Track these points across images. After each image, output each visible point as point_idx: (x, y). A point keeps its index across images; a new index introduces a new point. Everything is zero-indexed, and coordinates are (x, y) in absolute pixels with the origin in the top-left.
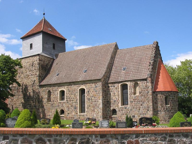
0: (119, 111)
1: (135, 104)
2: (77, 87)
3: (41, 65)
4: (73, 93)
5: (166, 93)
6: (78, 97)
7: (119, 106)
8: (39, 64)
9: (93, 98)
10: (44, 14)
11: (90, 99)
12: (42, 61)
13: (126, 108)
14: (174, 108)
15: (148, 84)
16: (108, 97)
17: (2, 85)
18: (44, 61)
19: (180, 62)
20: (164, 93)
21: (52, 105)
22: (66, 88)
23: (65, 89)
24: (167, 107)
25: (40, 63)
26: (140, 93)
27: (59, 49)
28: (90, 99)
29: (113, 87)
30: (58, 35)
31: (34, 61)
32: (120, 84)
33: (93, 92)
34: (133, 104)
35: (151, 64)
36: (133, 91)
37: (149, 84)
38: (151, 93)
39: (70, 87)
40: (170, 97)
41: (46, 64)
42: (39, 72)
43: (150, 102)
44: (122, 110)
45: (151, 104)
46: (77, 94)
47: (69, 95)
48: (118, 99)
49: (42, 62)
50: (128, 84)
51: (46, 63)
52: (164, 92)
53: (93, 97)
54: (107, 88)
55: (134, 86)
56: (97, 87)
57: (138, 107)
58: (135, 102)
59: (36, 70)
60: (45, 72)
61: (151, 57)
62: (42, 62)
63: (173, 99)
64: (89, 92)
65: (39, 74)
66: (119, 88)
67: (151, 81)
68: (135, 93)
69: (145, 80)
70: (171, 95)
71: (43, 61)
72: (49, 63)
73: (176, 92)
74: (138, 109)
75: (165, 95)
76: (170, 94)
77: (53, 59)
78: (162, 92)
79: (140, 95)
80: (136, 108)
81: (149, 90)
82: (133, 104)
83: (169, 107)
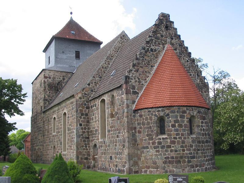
5: (159, 111)
10: (71, 13)
20: (154, 112)
24: (160, 139)
30: (86, 39)
40: (168, 118)
41: (57, 82)
51: (57, 80)
52: (154, 109)
63: (176, 121)
70: (170, 114)
72: (64, 79)
73: (188, 108)
76: (167, 112)
83: (166, 138)
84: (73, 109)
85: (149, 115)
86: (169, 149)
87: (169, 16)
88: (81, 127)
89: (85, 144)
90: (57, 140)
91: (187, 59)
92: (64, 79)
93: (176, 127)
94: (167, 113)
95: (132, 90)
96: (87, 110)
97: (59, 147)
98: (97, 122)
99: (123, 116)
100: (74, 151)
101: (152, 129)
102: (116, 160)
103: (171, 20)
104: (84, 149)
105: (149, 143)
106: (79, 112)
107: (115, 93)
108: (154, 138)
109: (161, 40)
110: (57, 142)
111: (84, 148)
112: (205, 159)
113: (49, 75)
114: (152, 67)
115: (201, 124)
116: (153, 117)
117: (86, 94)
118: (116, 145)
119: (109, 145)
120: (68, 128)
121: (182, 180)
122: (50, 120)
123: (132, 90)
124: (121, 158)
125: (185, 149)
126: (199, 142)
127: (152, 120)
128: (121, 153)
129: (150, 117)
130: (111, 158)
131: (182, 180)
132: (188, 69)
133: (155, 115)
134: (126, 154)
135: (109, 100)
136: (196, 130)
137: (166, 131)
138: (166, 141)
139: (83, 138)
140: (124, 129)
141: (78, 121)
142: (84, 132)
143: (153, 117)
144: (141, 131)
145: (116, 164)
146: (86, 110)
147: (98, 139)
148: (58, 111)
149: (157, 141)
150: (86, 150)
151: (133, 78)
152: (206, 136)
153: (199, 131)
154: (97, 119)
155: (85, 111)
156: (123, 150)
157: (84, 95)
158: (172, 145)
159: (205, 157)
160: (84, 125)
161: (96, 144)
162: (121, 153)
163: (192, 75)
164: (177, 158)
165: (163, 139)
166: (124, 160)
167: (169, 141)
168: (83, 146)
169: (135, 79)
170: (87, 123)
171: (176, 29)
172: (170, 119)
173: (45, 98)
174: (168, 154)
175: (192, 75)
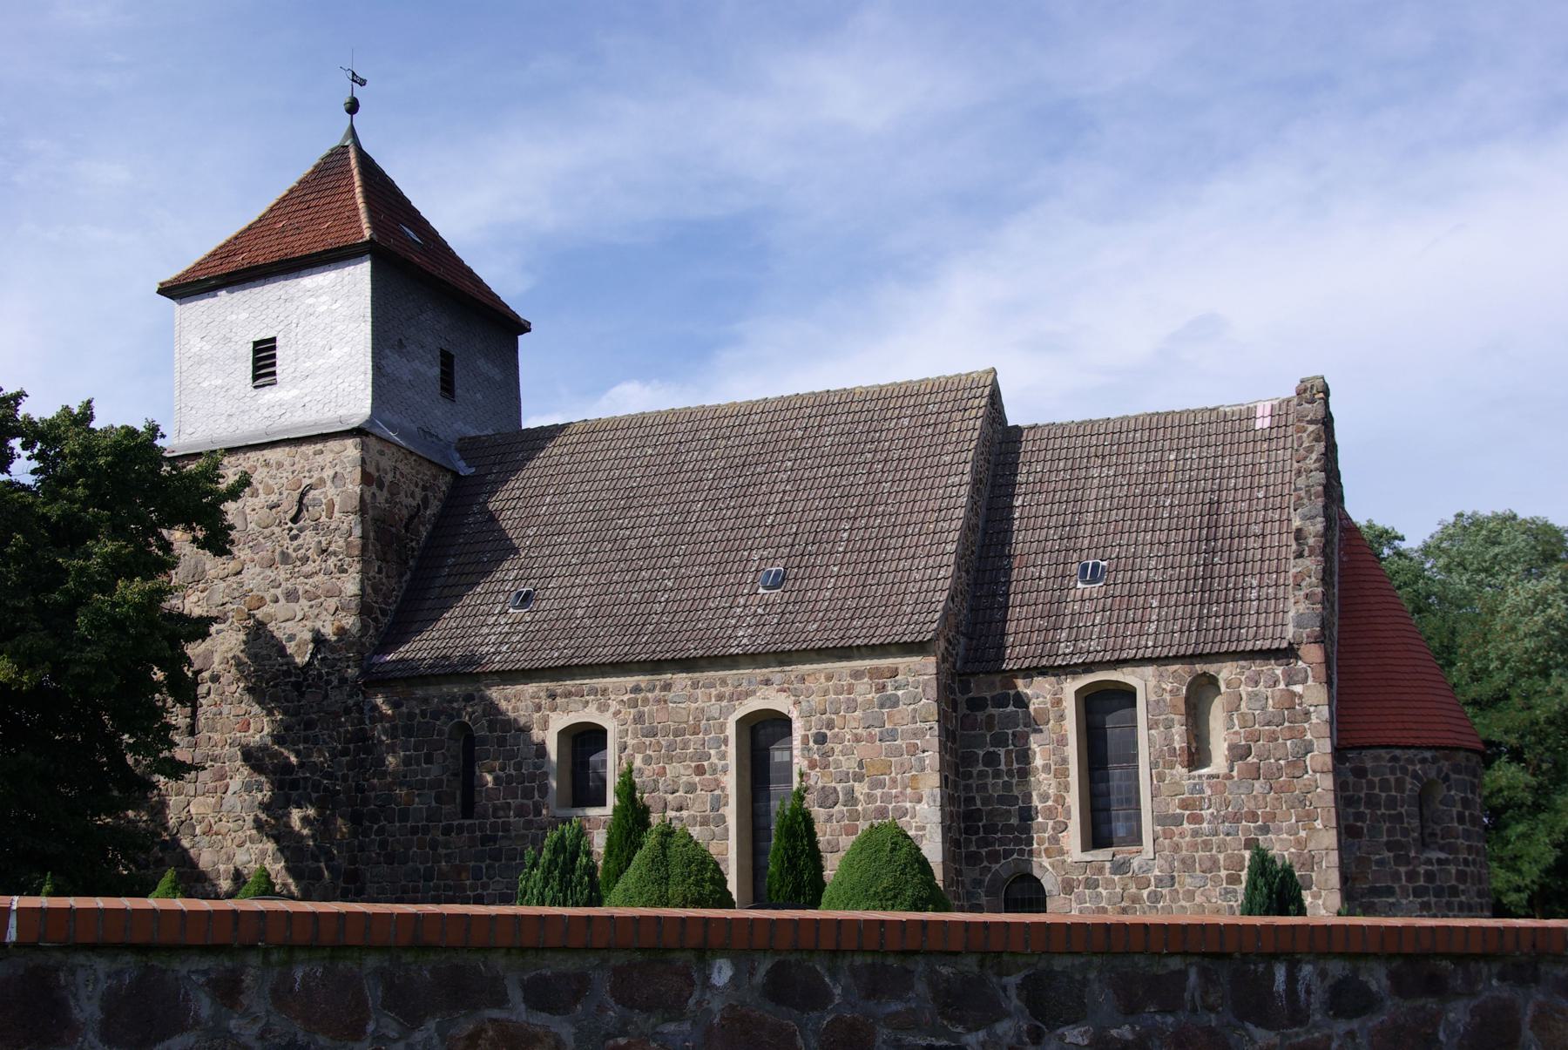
0: (1068, 887)
1: (1195, 833)
2: (720, 698)
3: (375, 520)
4: (685, 746)
6: (730, 781)
7: (1062, 852)
8: (363, 508)
9: (861, 789)
10: (353, 107)
11: (832, 797)
12: (381, 486)
13: (1120, 867)
14: (1472, 872)
15: (1298, 688)
16: (973, 782)
17: (1558, 628)
18: (394, 489)
19: (1400, 534)
21: (485, 840)
22: (614, 706)
23: (609, 714)
24: (1429, 862)
25: (368, 499)
26: (1238, 753)
27: (479, 396)
28: (832, 797)
29: (1011, 708)
31: (308, 481)
32: (1071, 686)
33: (857, 739)
34: (1182, 835)
35: (1311, 541)
36: (1176, 737)
37: (1314, 695)
38: (1329, 759)
39: (658, 701)
40: (1449, 788)
41: (405, 512)
42: (362, 571)
43: (1318, 824)
44: (1091, 884)
45: (1330, 839)
46: (723, 756)
47: (647, 760)
48: (1060, 800)
49: (382, 496)
50: (1137, 678)
52: (1411, 753)
53: (859, 778)
54: (965, 716)
55: (1187, 699)
56: (894, 701)
57: (1221, 857)
58: (1195, 819)
59: (335, 554)
60: (401, 575)
61: (1303, 493)
62: (378, 493)
64: (829, 745)
65: (362, 589)
66: (1062, 717)
67: (1322, 670)
68: (1197, 756)
69: (1288, 653)
70: (1454, 776)
71: (385, 489)
74: (1223, 873)
75: (1415, 776)
77: (448, 478)
78: (1398, 752)
79: (1235, 773)
80: (1208, 864)
81: (1309, 737)
82: (1182, 835)
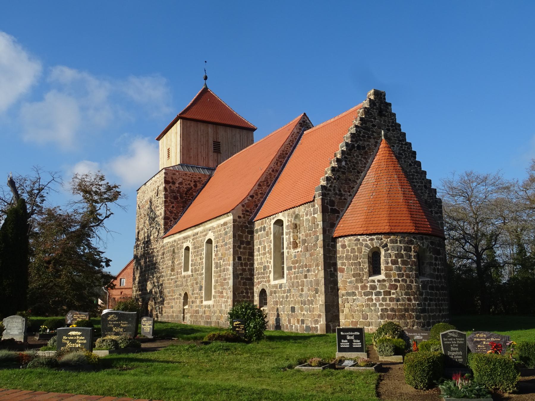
5: (372, 240)
10: (206, 78)
24: (373, 281)
76: (385, 240)
83: (384, 281)
84: (226, 233)
85: (356, 245)
86: (388, 297)
87: (385, 95)
88: (240, 262)
89: (246, 289)
90: (193, 283)
91: (410, 162)
92: (195, 186)
93: (398, 264)
94: (385, 242)
95: (330, 207)
96: (250, 236)
97: (197, 294)
98: (267, 254)
99: (315, 245)
100: (228, 299)
101: (361, 266)
102: (302, 313)
103: (387, 101)
104: (244, 297)
105: (357, 288)
106: (237, 238)
107: (302, 210)
108: (364, 280)
109: (373, 132)
110: (193, 286)
111: (244, 294)
112: (441, 314)
113: (172, 178)
114: (358, 172)
115: (434, 262)
116: (363, 248)
117: (247, 211)
118: (302, 290)
119: (289, 291)
120: (216, 264)
121: (422, 338)
122: (176, 251)
123: (330, 207)
124: (311, 309)
125: (412, 297)
126: (432, 288)
127: (361, 253)
128: (311, 302)
129: (358, 248)
130: (293, 309)
131: (422, 338)
132: (411, 177)
133: (367, 246)
134: (321, 303)
135: (291, 222)
136: (428, 270)
137: (383, 270)
138: (383, 285)
139: (242, 279)
140: (317, 265)
141: (235, 253)
142: (244, 270)
143: (363, 248)
144: (344, 269)
145: (302, 318)
146: (248, 236)
147: (269, 281)
148: (195, 236)
149: (368, 285)
150: (247, 298)
151: (332, 189)
152: (441, 280)
153: (432, 272)
154: (267, 250)
155: (246, 237)
156: (315, 297)
157: (244, 212)
158: (393, 291)
159: (440, 312)
160: (245, 259)
161: (265, 288)
162: (311, 302)
163: (417, 186)
164: (400, 310)
165: (379, 281)
166: (317, 313)
167: (387, 284)
168: (242, 292)
169: (334, 190)
170: (249, 255)
171: (394, 115)
172: (389, 252)
173: (167, 215)
174: (387, 305)
175: (417, 186)
